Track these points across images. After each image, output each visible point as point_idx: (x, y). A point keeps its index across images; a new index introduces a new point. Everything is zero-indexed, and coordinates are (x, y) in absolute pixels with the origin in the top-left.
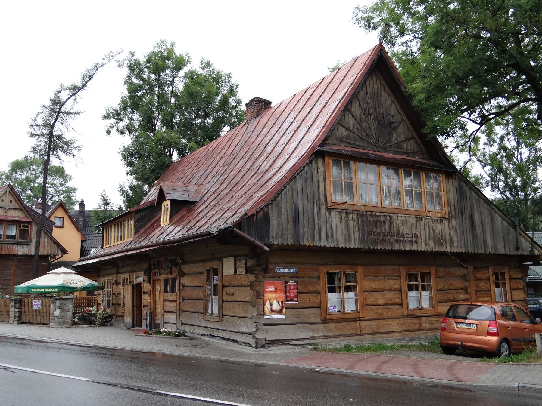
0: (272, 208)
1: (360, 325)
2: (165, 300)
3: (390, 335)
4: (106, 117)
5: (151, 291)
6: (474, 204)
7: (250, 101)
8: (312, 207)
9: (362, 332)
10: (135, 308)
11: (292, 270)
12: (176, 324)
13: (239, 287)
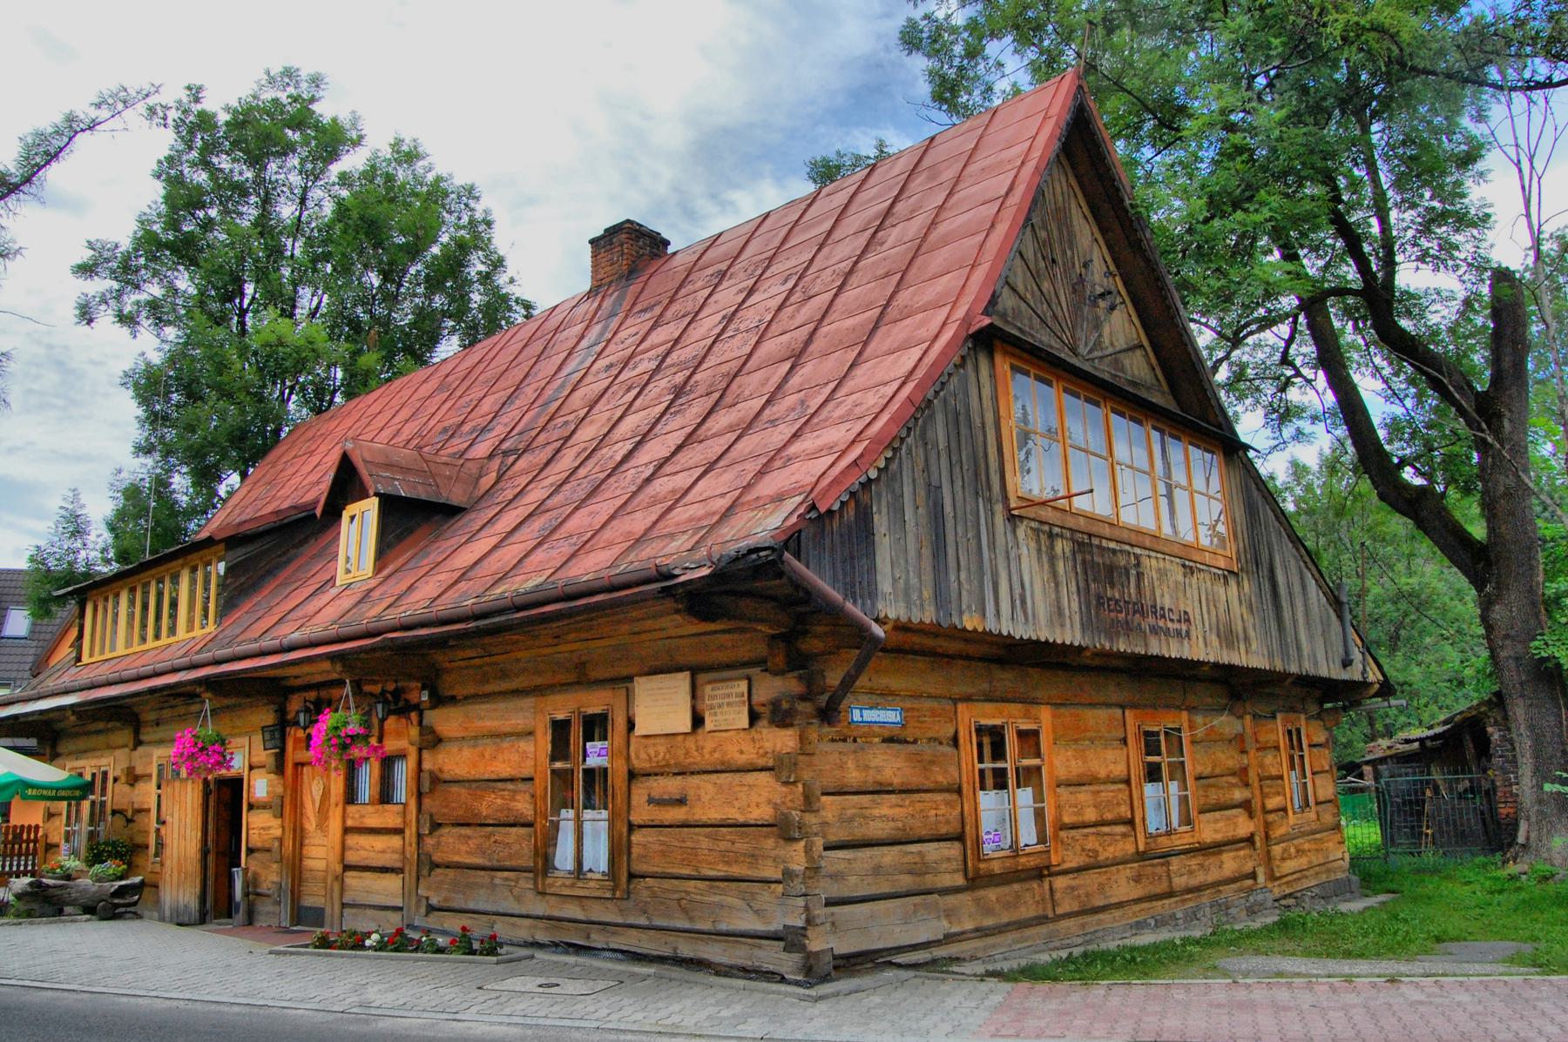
0: (879, 495)
1: (1051, 889)
2: (347, 831)
3: (1117, 913)
4: (86, 270)
5: (287, 800)
6: (1274, 539)
7: (606, 230)
8: (974, 505)
9: (1059, 911)
10: (211, 858)
11: (891, 716)
12: (401, 909)
13: (714, 776)
